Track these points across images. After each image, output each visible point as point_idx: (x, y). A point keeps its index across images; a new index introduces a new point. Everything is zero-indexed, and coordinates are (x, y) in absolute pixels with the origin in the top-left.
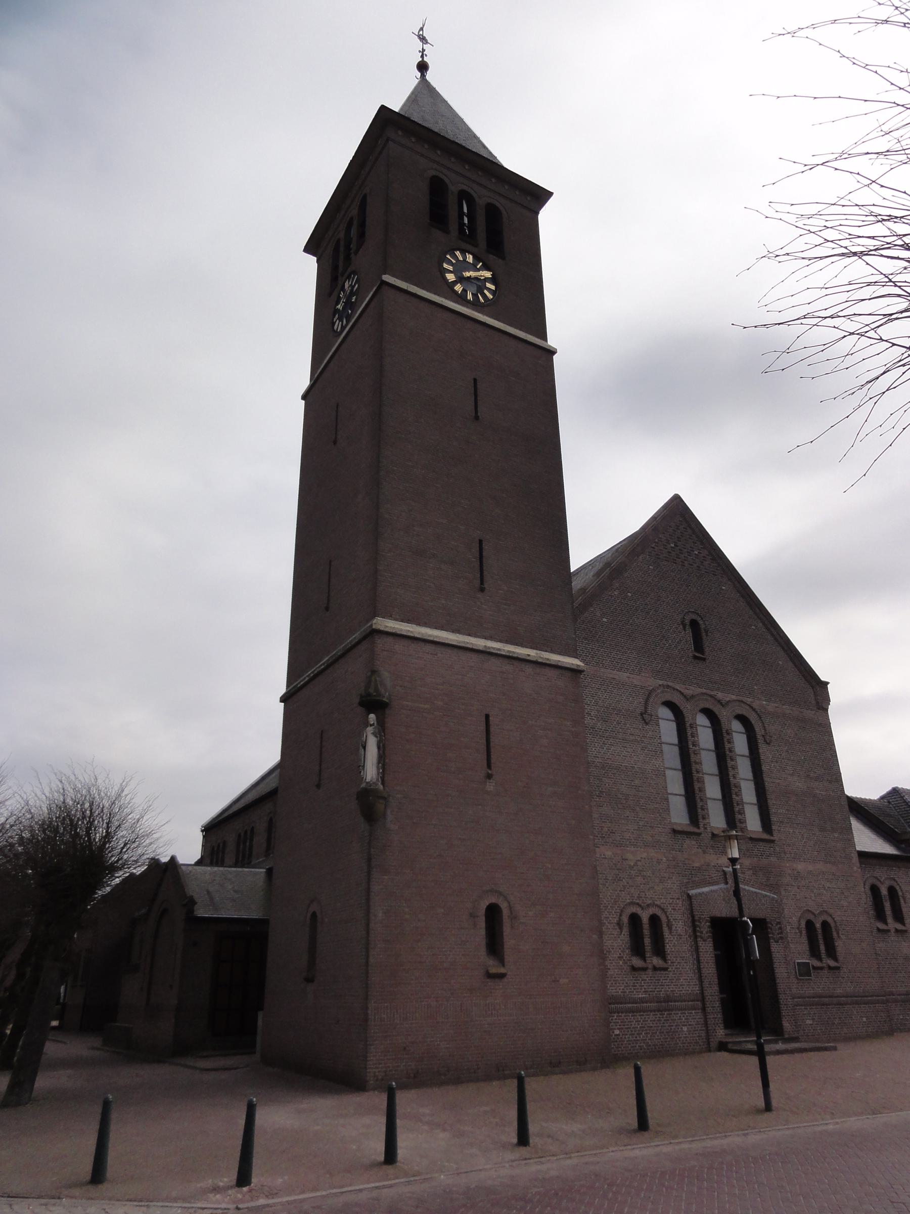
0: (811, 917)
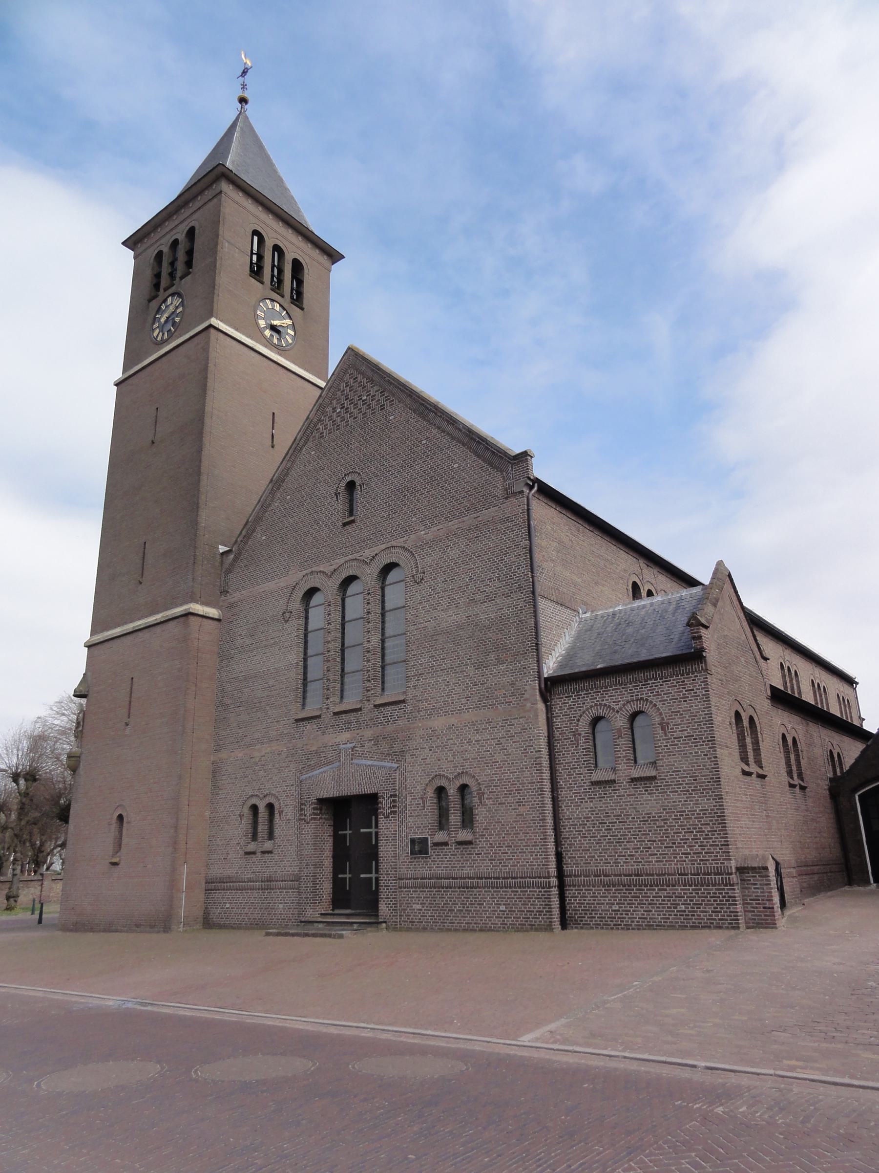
0: (443, 783)
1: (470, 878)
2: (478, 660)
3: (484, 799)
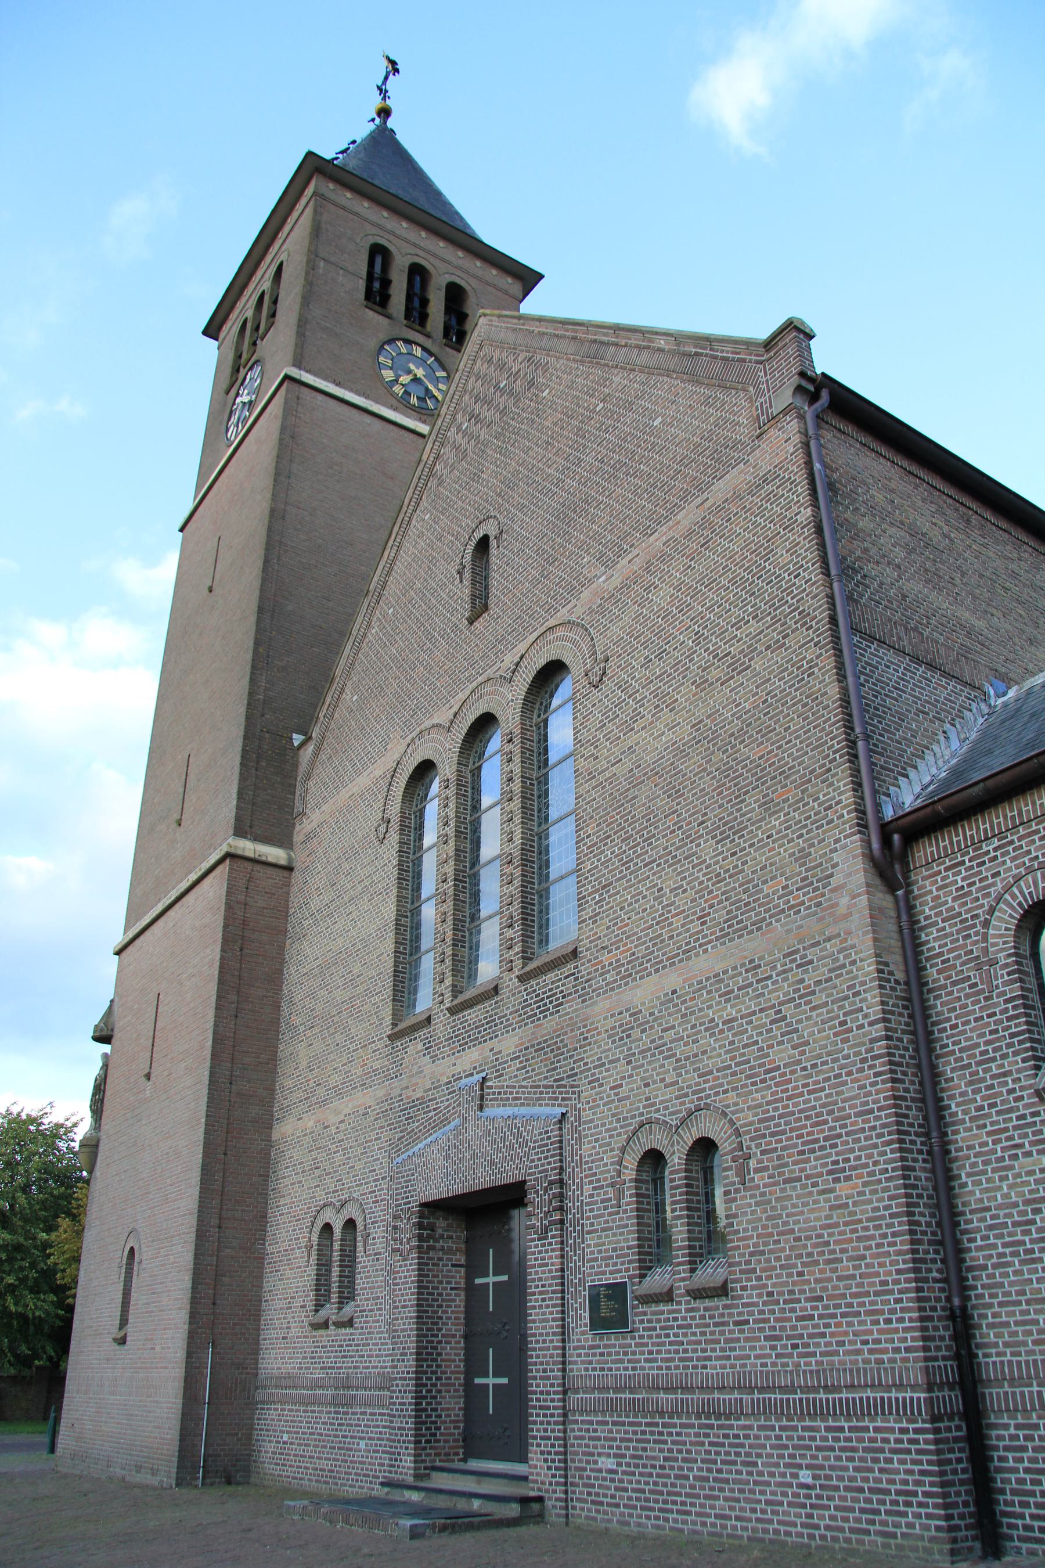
1: (722, 1389)
2: (720, 820)
3: (749, 1174)
